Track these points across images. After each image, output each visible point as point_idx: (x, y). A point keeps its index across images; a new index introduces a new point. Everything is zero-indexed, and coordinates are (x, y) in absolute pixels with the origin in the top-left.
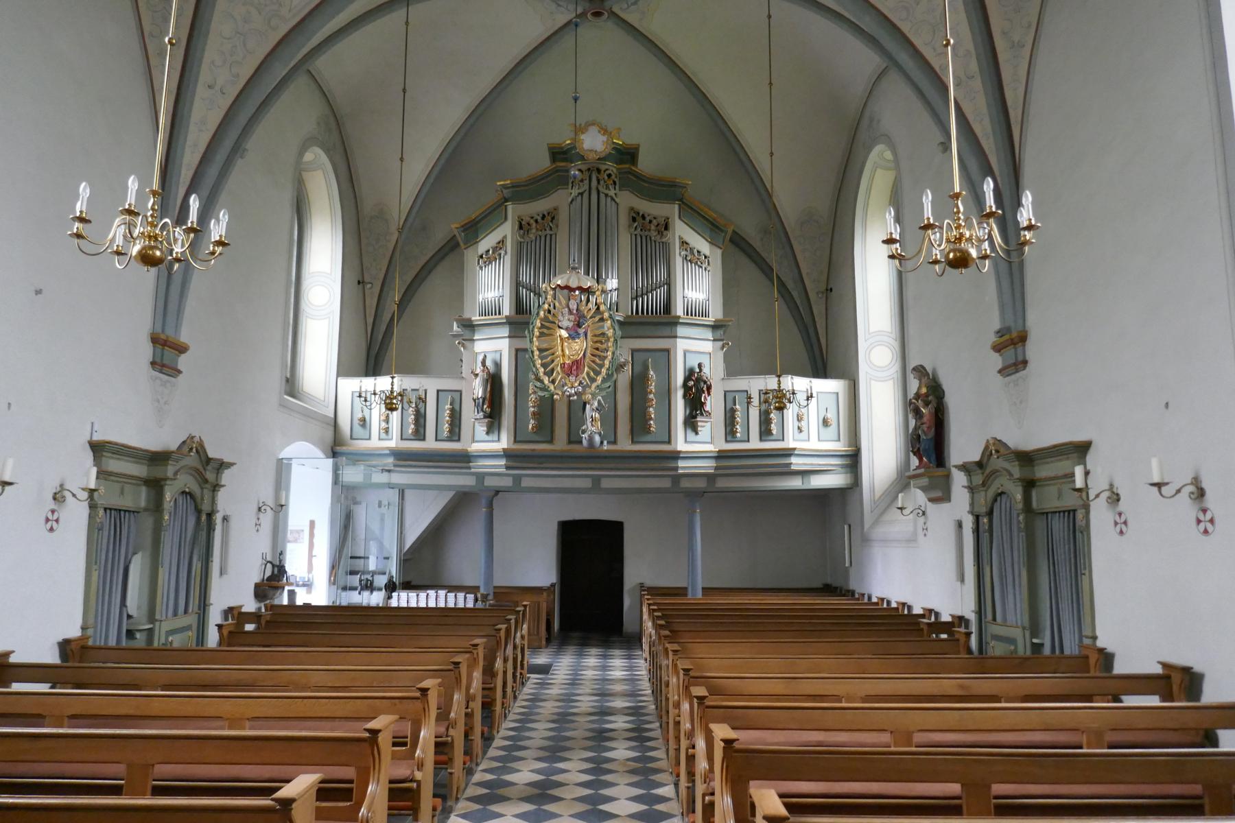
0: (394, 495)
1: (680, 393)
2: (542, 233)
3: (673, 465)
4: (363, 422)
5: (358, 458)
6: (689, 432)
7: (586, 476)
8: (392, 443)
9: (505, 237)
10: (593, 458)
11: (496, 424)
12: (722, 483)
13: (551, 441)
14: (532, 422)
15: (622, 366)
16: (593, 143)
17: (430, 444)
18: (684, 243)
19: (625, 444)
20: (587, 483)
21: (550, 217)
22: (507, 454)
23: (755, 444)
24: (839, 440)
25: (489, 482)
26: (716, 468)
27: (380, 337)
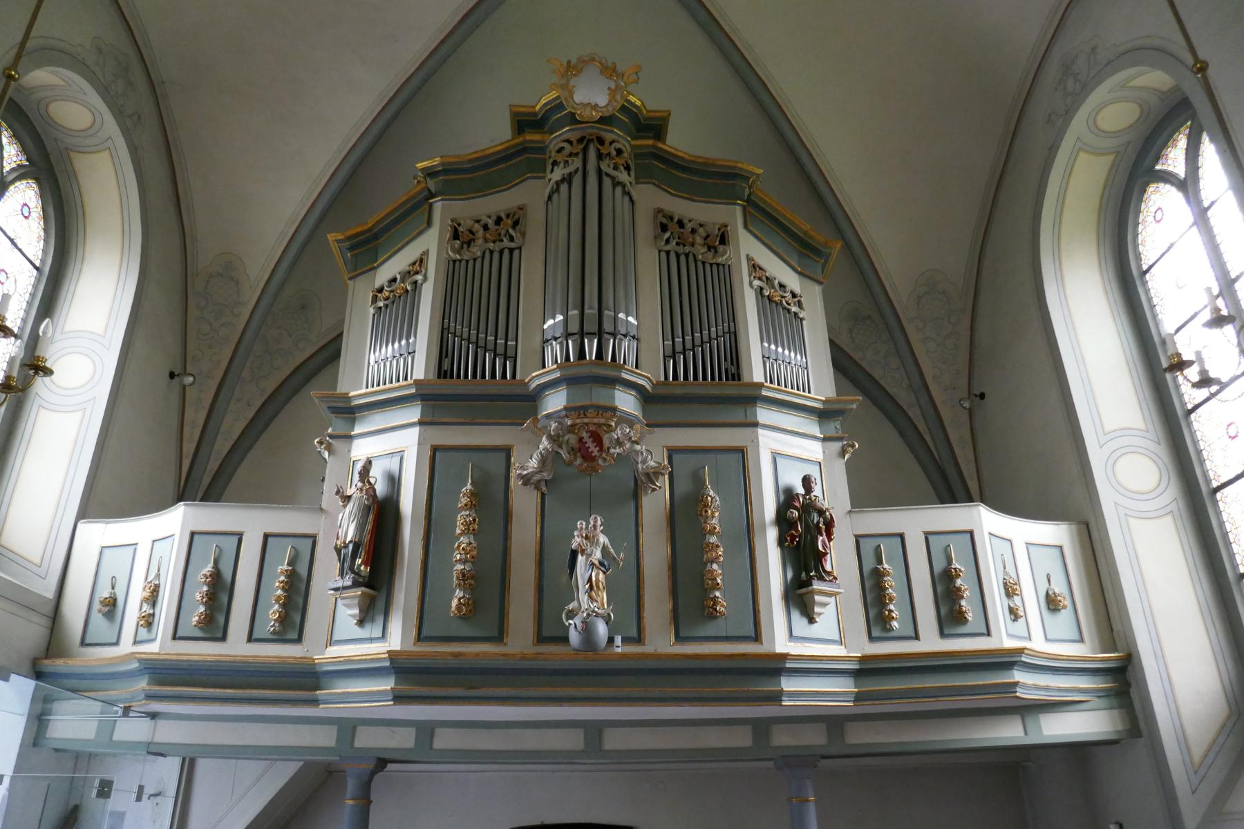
0: (167, 772)
1: (772, 534)
2: (496, 247)
3: (766, 687)
4: (111, 607)
5: (82, 684)
6: (799, 622)
8: (153, 648)
9: (426, 253)
10: (594, 676)
11: (380, 604)
12: (859, 736)
14: (459, 593)
15: (652, 476)
16: (592, 95)
17: (236, 647)
18: (755, 267)
19: (661, 641)
20: (573, 741)
21: (516, 219)
22: (399, 666)
23: (931, 642)
24: (1081, 640)
25: (366, 739)
26: (859, 698)
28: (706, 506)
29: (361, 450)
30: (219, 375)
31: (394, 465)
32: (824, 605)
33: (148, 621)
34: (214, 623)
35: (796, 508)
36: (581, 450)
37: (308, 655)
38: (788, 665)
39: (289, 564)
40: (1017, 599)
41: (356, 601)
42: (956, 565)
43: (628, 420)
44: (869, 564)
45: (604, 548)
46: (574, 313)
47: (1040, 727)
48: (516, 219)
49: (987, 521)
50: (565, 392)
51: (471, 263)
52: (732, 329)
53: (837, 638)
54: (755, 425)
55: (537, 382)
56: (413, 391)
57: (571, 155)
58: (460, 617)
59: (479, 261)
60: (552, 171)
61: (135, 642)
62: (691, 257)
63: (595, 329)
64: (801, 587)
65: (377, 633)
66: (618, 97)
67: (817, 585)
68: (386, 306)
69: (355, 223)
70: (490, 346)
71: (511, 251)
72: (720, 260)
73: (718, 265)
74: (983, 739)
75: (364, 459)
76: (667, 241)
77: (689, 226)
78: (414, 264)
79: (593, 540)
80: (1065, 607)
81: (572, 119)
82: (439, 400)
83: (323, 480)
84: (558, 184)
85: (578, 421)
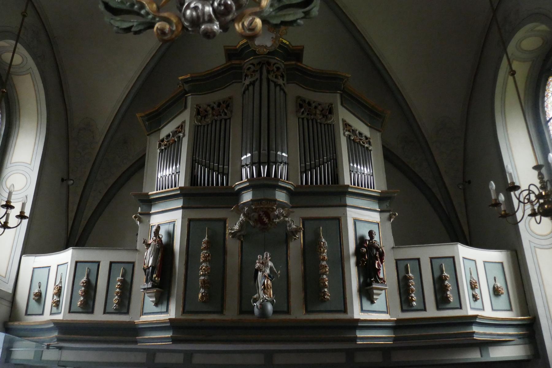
1: (353, 261)
2: (218, 118)
4: (39, 297)
6: (365, 301)
7: (340, 350)
8: (60, 317)
9: (184, 122)
12: (399, 358)
13: (221, 312)
14: (202, 290)
15: (295, 232)
18: (347, 125)
19: (298, 313)
21: (227, 104)
22: (173, 325)
23: (432, 312)
24: (511, 310)
26: (395, 339)
27: (80, 230)
28: (320, 247)
29: (155, 220)
30: (85, 180)
31: (171, 227)
32: (379, 294)
33: (57, 304)
34: (88, 306)
35: (365, 247)
36: (259, 220)
37: (132, 320)
38: (359, 325)
39: (122, 276)
40: (477, 291)
41: (153, 294)
42: (445, 274)
43: (282, 205)
44: (402, 274)
45: (271, 268)
46: (256, 153)
47: (489, 354)
48: (227, 104)
49: (463, 251)
50: (251, 192)
51: (206, 127)
52: (335, 158)
53: (385, 310)
54: (345, 206)
55: (238, 187)
56: (179, 192)
57: (254, 71)
58: (203, 302)
59: (210, 125)
60: (245, 79)
61: (51, 314)
62: (314, 120)
63: (266, 161)
64: (367, 286)
65: (164, 309)
66: (277, 42)
67: (375, 285)
68: (165, 149)
69: (149, 106)
70: (216, 169)
71: (226, 120)
72: (329, 122)
73: (328, 124)
74: (463, 359)
75: (157, 224)
76: (303, 113)
77: (313, 105)
78: (178, 127)
79: (266, 265)
80: (502, 293)
81: (254, 53)
82: (192, 196)
83: (137, 234)
84: (248, 86)
85: (258, 207)
